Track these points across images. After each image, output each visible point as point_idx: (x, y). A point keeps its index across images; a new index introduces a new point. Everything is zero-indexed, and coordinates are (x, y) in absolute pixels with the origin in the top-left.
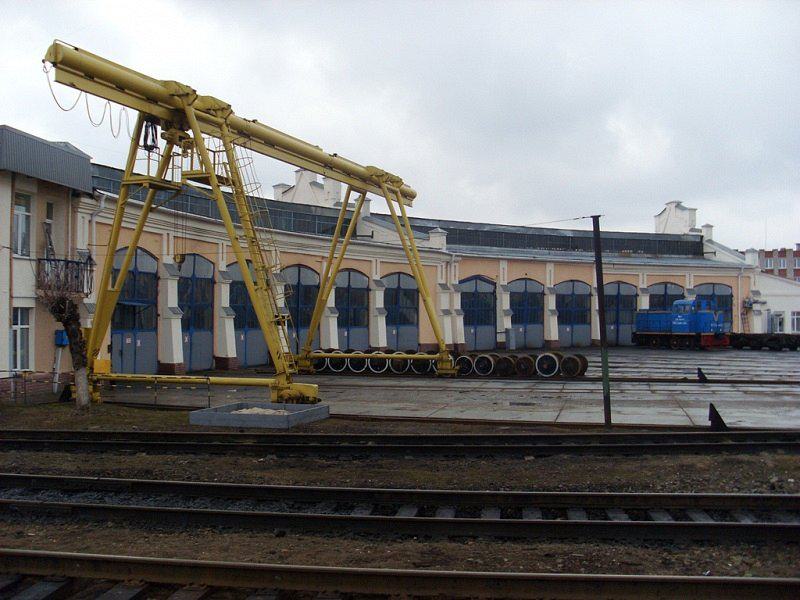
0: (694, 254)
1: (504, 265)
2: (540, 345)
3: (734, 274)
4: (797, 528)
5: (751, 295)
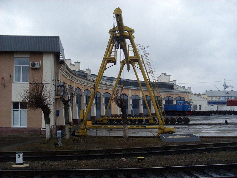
0: (171, 88)
1: (130, 90)
2: (138, 115)
3: (185, 94)
4: (236, 165)
5: (189, 100)
